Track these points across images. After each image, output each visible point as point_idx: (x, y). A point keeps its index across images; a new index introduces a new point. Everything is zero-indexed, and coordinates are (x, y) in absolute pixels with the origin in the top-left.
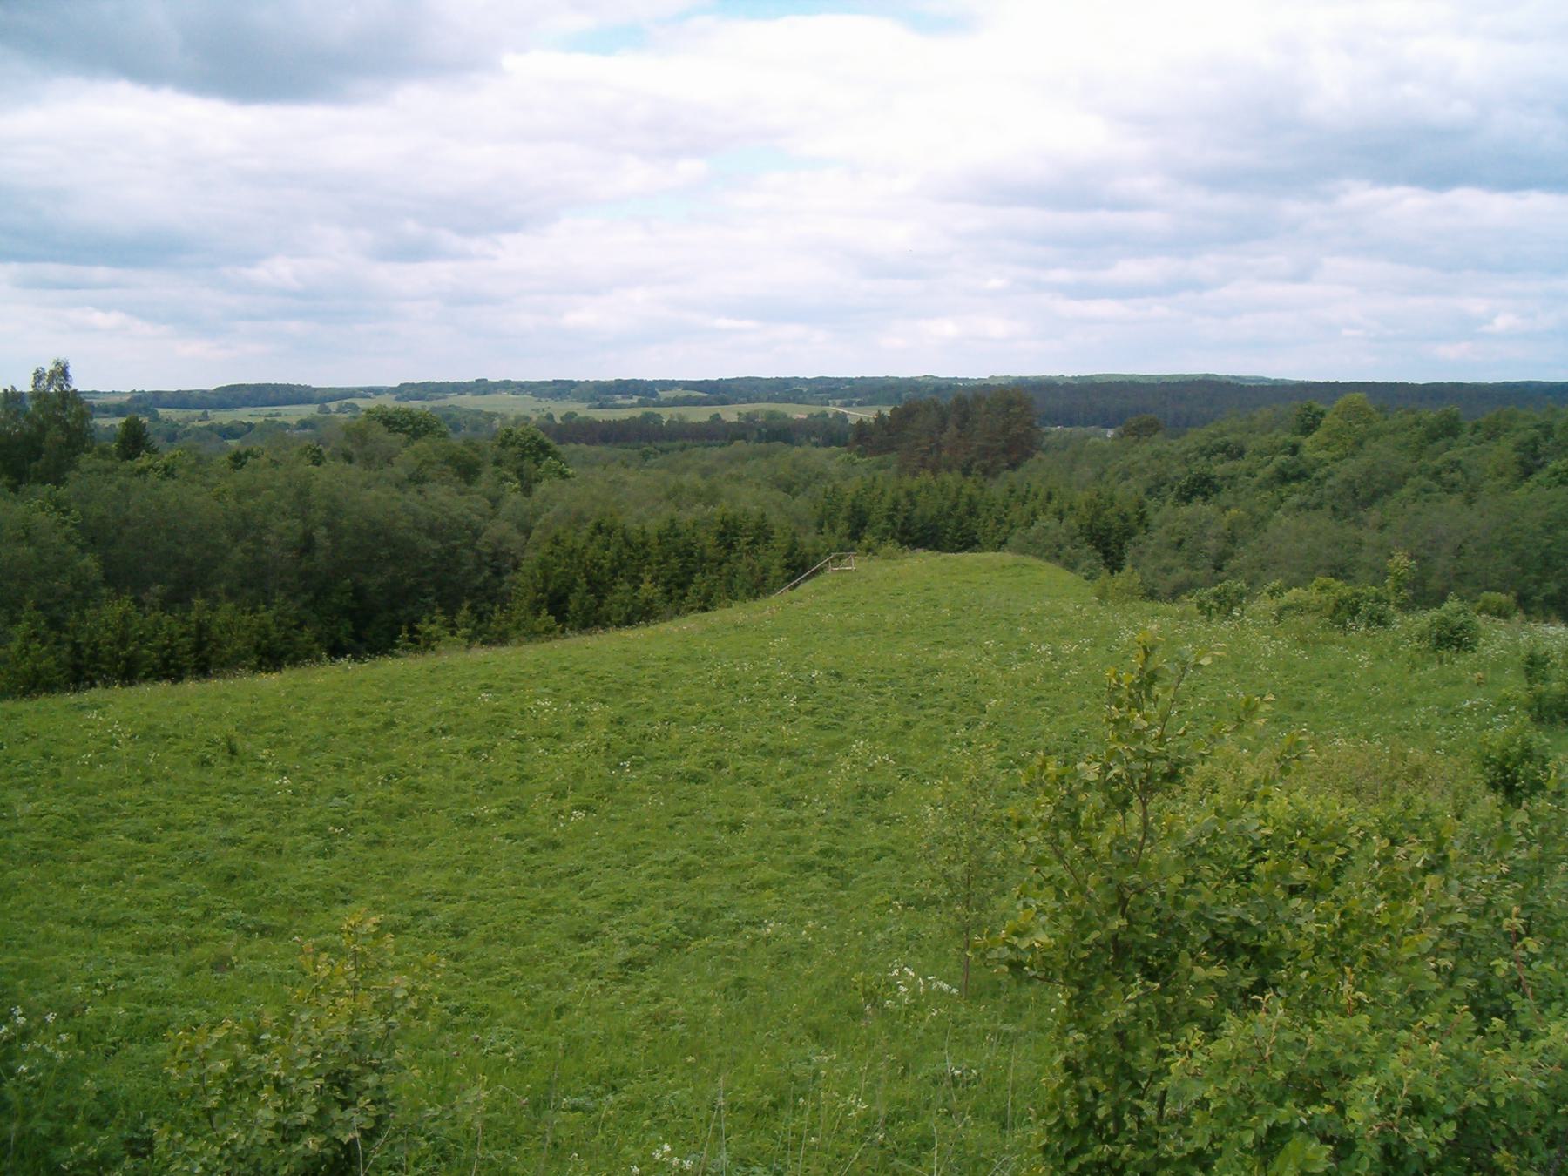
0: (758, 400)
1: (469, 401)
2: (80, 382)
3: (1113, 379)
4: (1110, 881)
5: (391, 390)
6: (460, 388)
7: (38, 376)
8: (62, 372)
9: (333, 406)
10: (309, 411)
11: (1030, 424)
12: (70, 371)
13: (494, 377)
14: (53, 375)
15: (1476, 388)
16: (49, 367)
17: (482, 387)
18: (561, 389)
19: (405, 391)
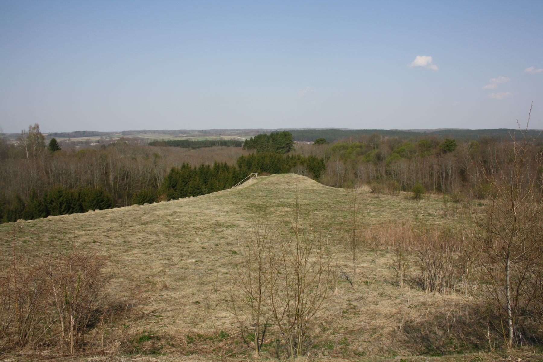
0: (231, 136)
1: (141, 136)
2: (45, 130)
3: (416, 131)
4: (463, 174)
5: (120, 132)
6: (139, 132)
7: (30, 127)
8: (37, 127)
9: (104, 137)
10: (98, 138)
11: (291, 141)
12: (40, 127)
13: (147, 129)
14: (34, 128)
15: (386, 131)
16: (33, 126)
17: (145, 132)
18: (164, 132)
19: (124, 133)
